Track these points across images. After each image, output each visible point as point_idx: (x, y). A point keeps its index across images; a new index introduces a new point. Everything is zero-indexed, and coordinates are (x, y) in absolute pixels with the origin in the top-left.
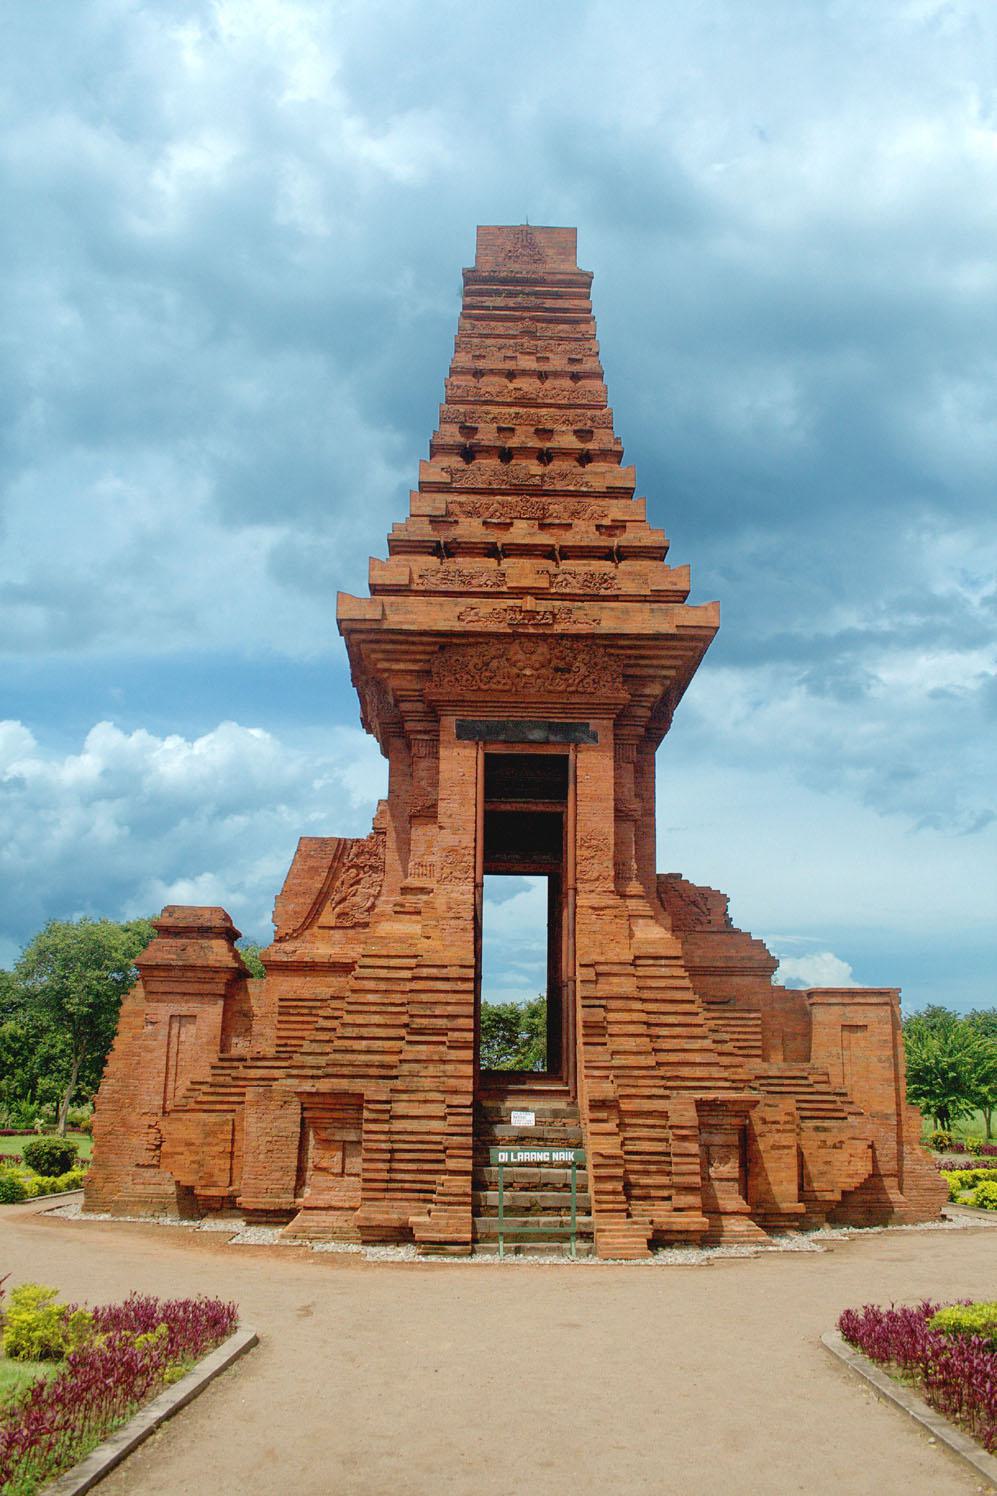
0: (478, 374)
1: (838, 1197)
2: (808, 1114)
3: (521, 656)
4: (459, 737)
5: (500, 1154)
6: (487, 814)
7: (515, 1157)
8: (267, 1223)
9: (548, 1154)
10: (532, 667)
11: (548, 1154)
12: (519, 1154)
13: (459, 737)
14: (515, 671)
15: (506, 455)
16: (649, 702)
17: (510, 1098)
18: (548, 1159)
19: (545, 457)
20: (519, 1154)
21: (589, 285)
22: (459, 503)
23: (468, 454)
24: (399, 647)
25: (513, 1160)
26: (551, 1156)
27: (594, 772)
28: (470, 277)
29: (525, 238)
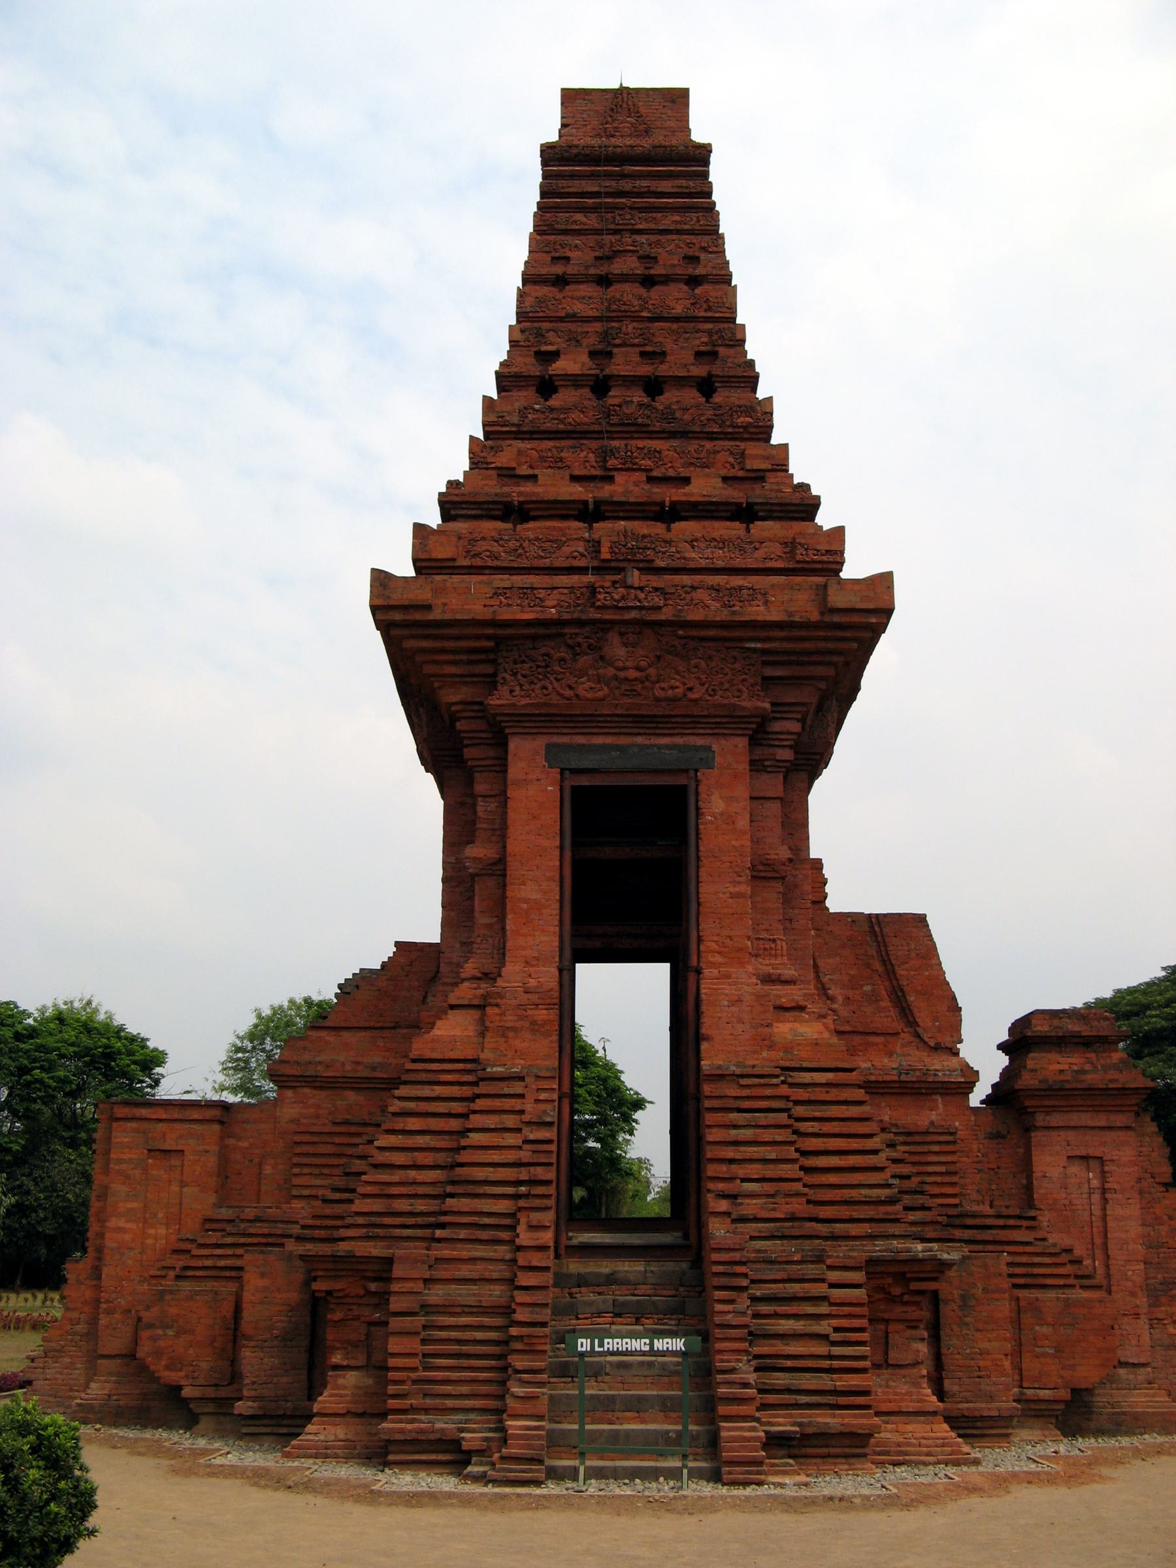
0: (560, 281)
1: (1064, 1394)
2: (1022, 1281)
3: (621, 652)
4: (578, 793)
5: (580, 1341)
6: (576, 864)
7: (601, 1345)
8: (242, 1436)
9: (647, 1341)
10: (638, 669)
11: (647, 1341)
12: (606, 1341)
13: (578, 793)
14: (611, 671)
15: (601, 387)
16: (798, 712)
17: (402, 1087)
18: (647, 1348)
19: (653, 387)
20: (606, 1341)
21: (706, 162)
22: (712, 588)
23: (546, 387)
24: (436, 632)
25: (597, 1349)
26: (652, 1344)
27: (723, 808)
28: (549, 154)
29: (622, 101)
